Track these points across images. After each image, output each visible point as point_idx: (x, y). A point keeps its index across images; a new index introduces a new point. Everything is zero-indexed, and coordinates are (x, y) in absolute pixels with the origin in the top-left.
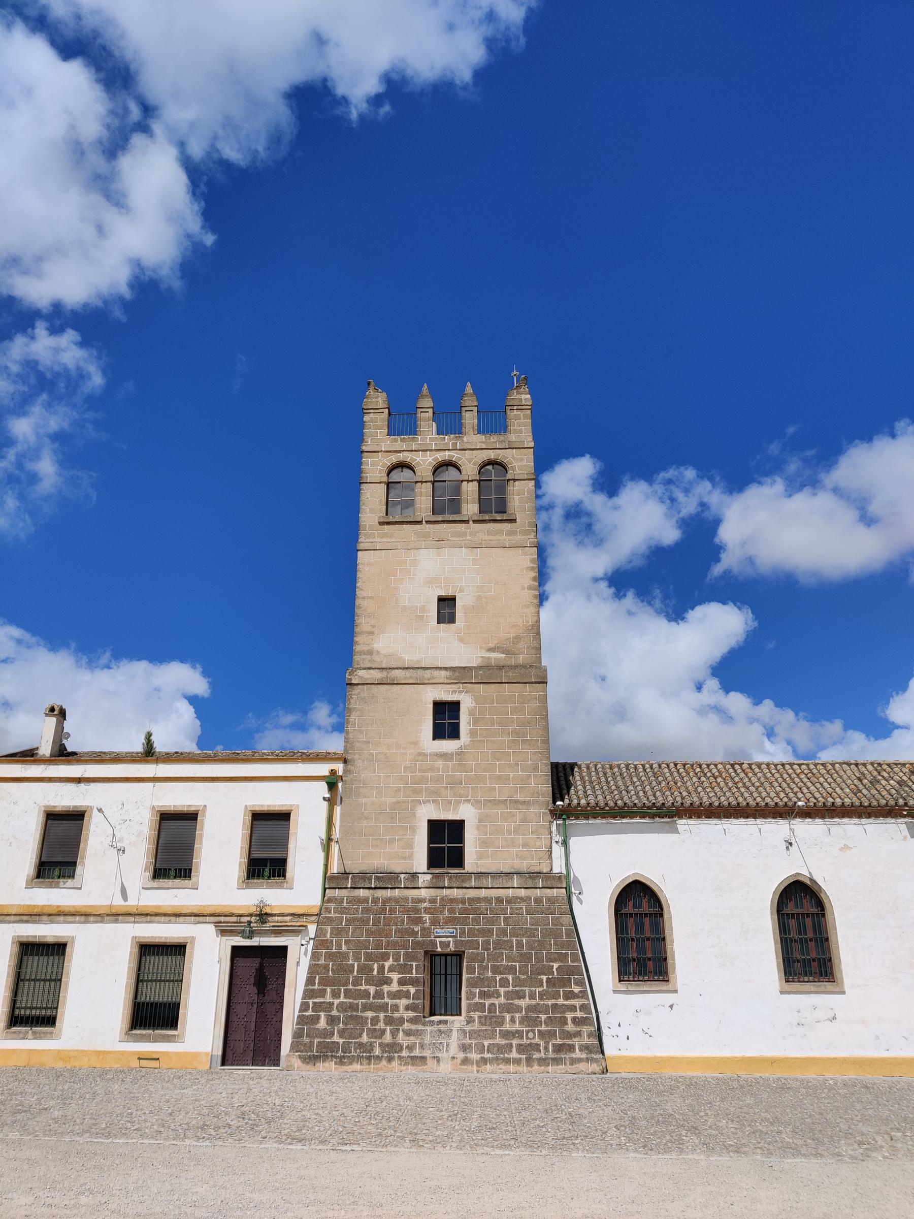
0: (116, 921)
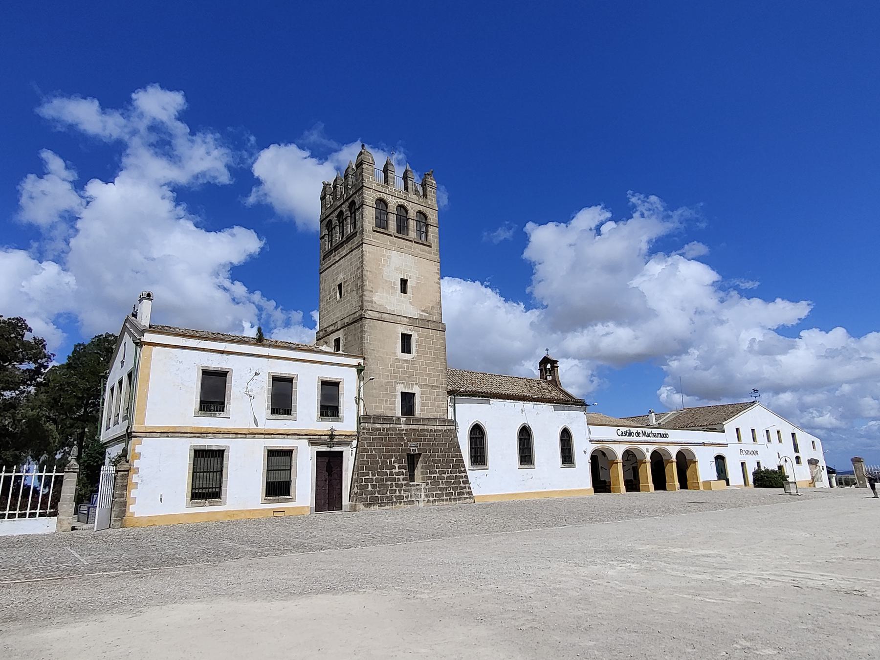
0: (254, 437)
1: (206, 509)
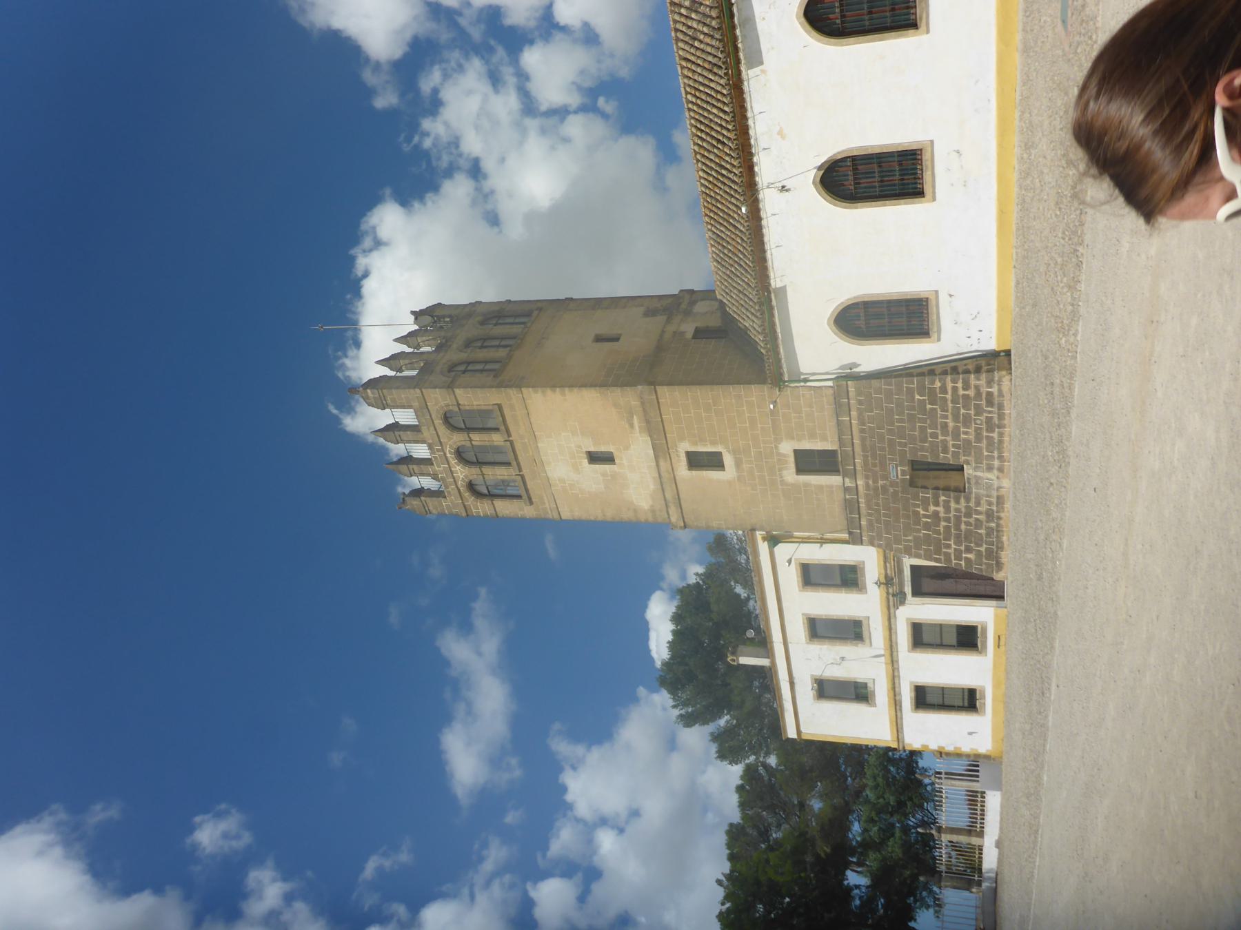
1: (989, 701)
